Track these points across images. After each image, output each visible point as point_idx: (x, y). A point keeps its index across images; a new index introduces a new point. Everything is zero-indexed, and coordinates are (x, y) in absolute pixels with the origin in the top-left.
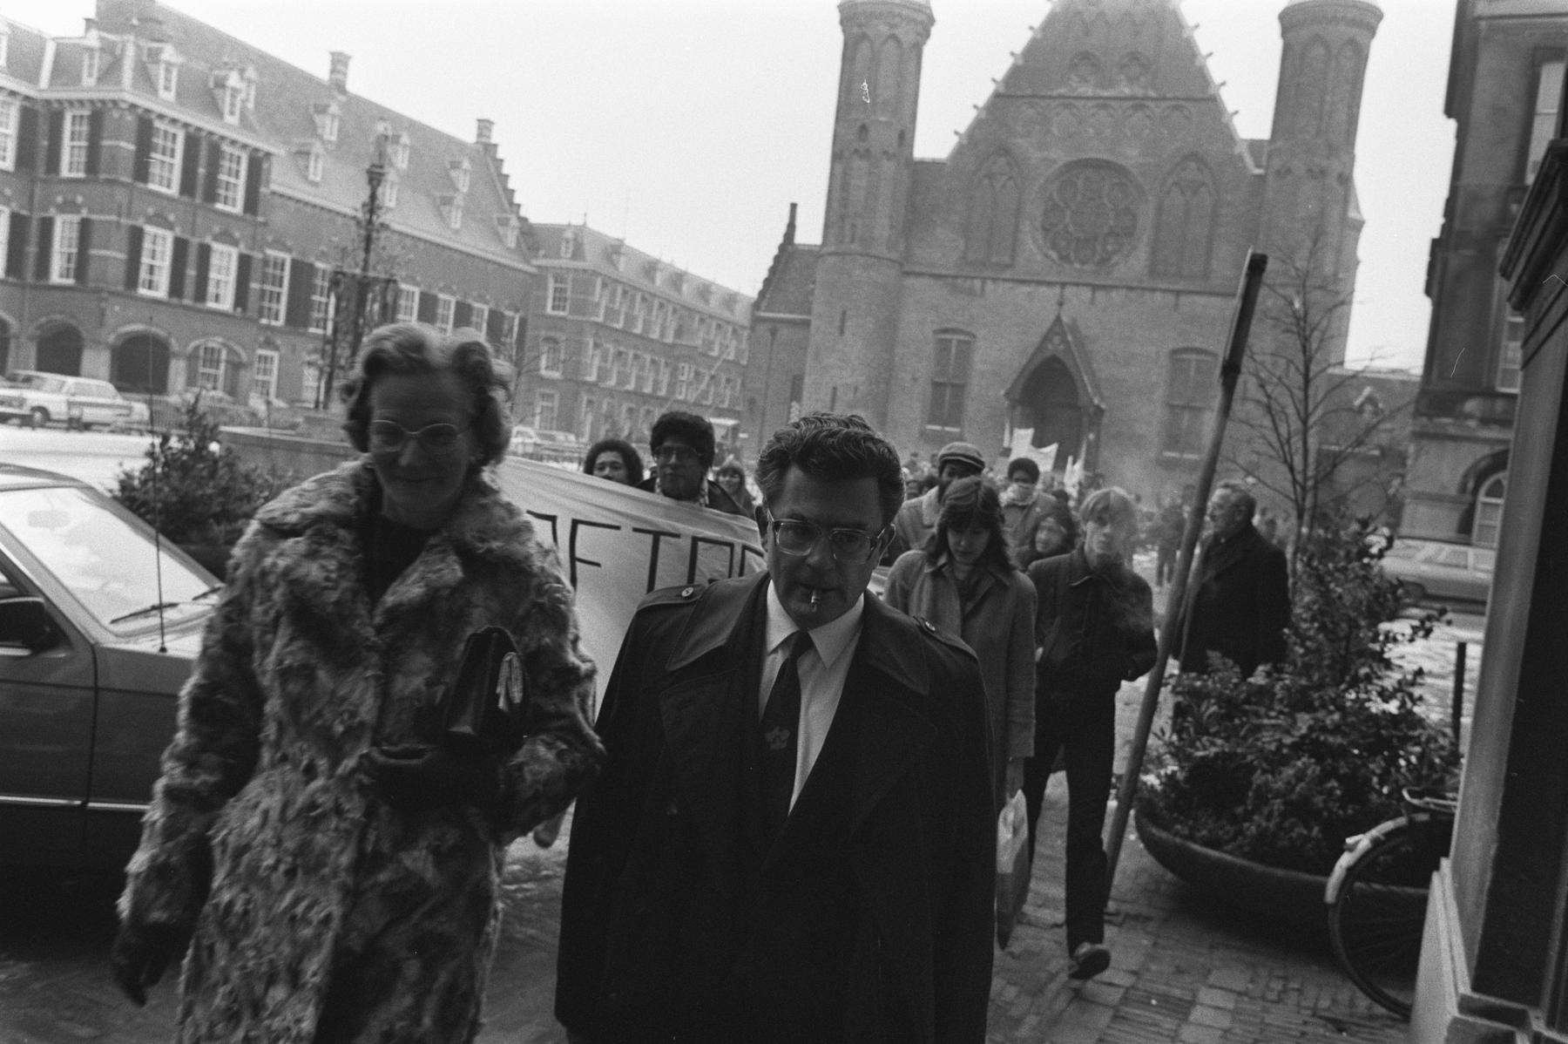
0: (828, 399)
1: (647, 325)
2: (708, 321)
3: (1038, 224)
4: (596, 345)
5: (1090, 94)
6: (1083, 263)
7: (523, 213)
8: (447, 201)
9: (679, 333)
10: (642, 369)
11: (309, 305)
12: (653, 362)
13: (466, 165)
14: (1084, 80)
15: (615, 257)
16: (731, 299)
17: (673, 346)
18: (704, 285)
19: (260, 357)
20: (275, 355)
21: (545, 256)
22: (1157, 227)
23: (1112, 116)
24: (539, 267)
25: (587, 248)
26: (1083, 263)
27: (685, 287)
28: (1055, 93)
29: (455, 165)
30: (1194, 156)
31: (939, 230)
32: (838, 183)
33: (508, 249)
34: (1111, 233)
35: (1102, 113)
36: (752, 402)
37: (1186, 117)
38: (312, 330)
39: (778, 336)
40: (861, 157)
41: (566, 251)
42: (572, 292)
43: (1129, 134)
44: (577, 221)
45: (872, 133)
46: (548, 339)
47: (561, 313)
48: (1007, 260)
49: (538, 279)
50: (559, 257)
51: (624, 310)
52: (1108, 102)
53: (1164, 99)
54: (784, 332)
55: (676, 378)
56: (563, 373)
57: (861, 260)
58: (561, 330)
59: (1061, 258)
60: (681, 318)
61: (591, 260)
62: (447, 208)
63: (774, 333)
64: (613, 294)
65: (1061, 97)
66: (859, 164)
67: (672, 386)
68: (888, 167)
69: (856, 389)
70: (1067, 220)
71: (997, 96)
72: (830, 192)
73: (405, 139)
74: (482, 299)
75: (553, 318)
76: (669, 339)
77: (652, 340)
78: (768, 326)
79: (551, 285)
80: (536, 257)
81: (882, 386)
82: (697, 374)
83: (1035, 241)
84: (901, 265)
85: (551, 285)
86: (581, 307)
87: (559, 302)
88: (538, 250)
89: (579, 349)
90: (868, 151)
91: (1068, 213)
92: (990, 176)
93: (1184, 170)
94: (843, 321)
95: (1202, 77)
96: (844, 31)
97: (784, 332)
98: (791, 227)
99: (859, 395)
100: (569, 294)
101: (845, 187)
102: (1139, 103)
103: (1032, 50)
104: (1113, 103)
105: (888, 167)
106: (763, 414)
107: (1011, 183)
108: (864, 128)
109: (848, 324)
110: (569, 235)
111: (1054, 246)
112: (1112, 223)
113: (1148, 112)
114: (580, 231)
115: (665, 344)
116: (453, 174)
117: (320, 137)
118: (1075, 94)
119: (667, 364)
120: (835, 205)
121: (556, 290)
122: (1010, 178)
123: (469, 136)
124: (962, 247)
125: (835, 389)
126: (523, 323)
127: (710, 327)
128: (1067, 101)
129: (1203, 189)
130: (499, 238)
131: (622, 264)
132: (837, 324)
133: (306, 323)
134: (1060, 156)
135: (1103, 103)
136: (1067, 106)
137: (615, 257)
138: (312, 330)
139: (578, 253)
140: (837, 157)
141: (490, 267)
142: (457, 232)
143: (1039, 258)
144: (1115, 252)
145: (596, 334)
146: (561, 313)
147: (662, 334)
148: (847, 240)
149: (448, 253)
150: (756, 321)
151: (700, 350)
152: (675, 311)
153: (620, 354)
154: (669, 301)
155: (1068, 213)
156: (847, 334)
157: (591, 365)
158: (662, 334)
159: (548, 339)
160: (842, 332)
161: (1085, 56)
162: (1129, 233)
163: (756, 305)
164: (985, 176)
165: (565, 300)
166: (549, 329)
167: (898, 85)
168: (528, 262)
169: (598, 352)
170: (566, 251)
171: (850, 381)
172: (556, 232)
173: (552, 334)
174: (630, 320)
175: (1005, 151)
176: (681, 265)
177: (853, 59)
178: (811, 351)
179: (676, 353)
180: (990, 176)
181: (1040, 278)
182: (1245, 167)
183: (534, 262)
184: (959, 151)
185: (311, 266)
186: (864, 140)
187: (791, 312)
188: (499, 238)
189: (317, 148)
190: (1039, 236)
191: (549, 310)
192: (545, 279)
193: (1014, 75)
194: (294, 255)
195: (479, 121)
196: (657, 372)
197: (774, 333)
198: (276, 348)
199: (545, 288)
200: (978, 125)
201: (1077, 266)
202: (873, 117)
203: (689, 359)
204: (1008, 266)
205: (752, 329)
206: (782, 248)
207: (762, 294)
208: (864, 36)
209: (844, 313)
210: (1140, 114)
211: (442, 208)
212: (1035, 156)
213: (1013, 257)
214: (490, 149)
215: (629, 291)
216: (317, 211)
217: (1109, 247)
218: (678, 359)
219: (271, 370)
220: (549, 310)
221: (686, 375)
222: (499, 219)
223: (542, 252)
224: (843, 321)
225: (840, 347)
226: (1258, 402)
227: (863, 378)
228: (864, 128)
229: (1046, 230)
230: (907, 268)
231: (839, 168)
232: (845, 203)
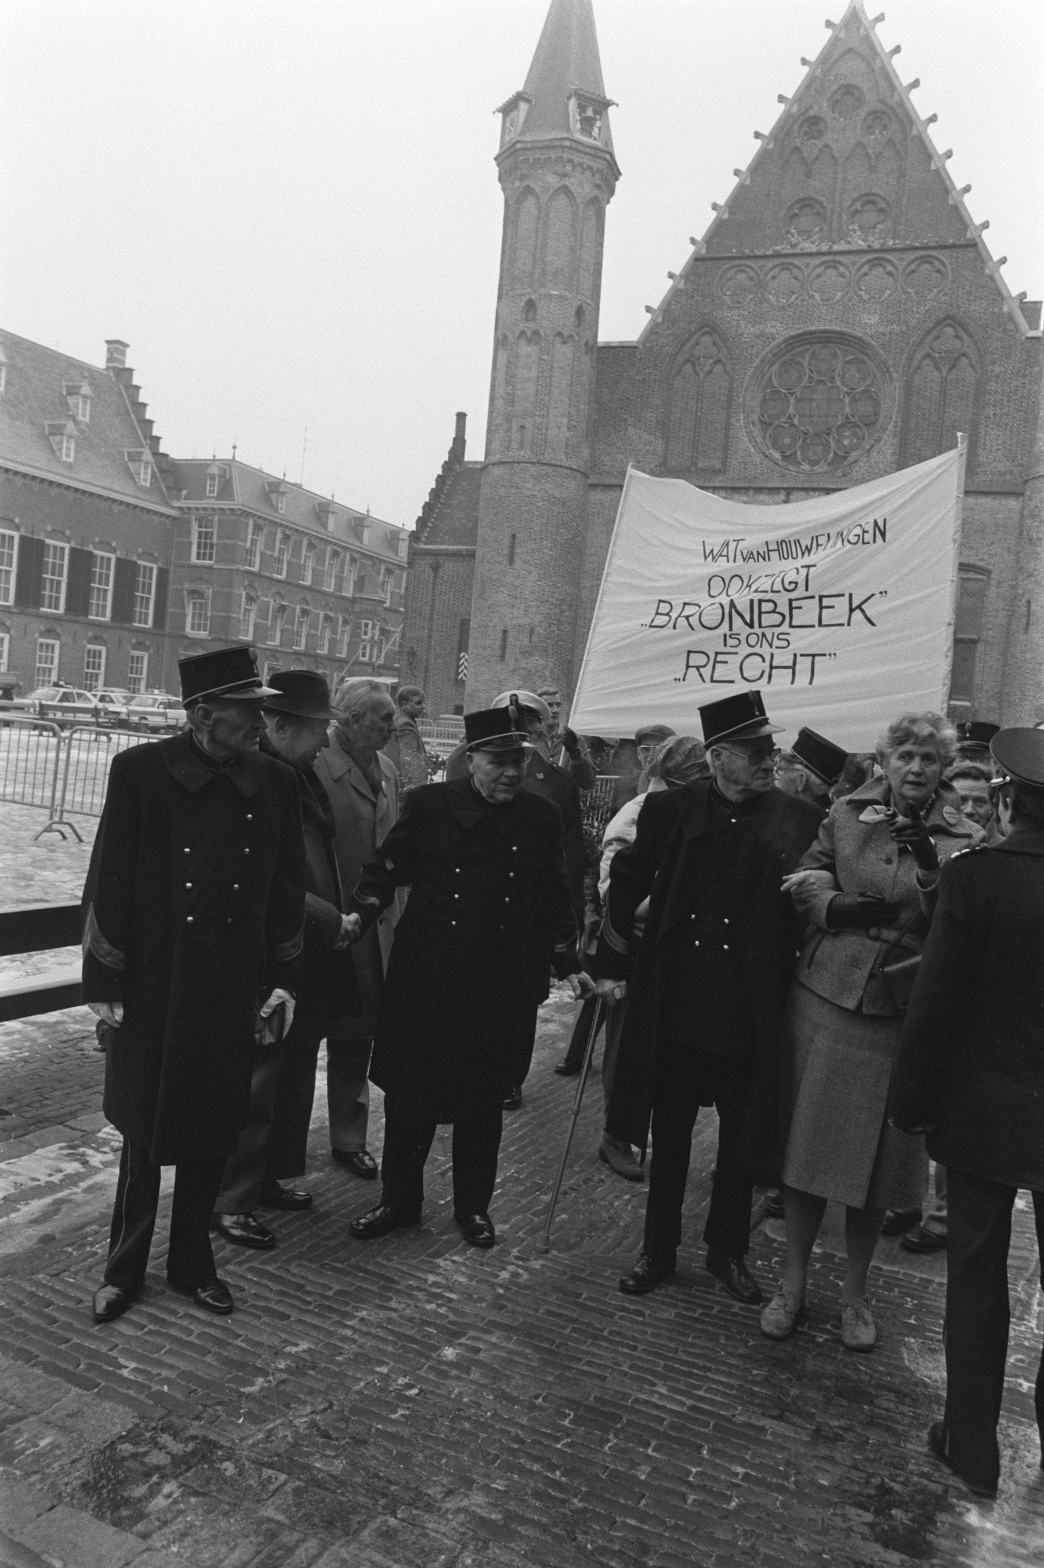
0: (498, 643)
1: (318, 576)
2: (295, 537)
3: (755, 417)
4: (251, 599)
5: (813, 248)
6: (812, 464)
7: (163, 449)
8: (57, 430)
9: (360, 585)
10: (314, 626)
11: (40, 583)
12: (327, 618)
13: (86, 390)
14: (806, 234)
15: (273, 497)
16: (392, 536)
17: (354, 600)
18: (320, 505)
19: (41, 645)
20: (57, 644)
21: (186, 498)
22: (906, 412)
23: (842, 276)
24: (181, 509)
25: (236, 485)
26: (812, 464)
27: (366, 534)
28: (770, 252)
29: (73, 391)
30: (950, 320)
31: (632, 432)
32: (501, 378)
33: (141, 488)
34: (848, 423)
35: (831, 273)
36: (412, 653)
37: (938, 271)
38: (44, 610)
39: (441, 572)
40: (529, 341)
41: (212, 489)
42: (219, 537)
43: (865, 297)
44: (225, 454)
45: (541, 311)
46: (193, 593)
47: (207, 562)
48: (718, 465)
49: (179, 524)
50: (205, 497)
51: (286, 557)
52: (838, 258)
53: (907, 249)
54: (449, 567)
55: (358, 636)
56: (210, 633)
57: (533, 469)
58: (209, 582)
59: (784, 457)
60: (363, 567)
61: (242, 497)
62: (58, 438)
63: (436, 568)
64: (272, 536)
65: (777, 255)
66: (527, 350)
67: (353, 646)
68: (564, 353)
69: (532, 631)
70: (791, 410)
71: (697, 259)
72: (493, 387)
73: (86, 390)
74: (105, 545)
75: (196, 567)
76: (349, 593)
77: (325, 594)
78: (431, 560)
79: (195, 529)
80: (179, 499)
81: (566, 628)
82: (383, 631)
83: (752, 438)
84: (586, 476)
85: (195, 529)
86: (229, 554)
87: (206, 547)
88: (180, 490)
89: (227, 602)
90: (536, 333)
91: (792, 400)
92: (692, 361)
93: (938, 337)
94: (512, 547)
95: (958, 216)
96: (504, 190)
97: (449, 567)
98: (459, 442)
99: (535, 638)
100: (215, 540)
101: (510, 380)
102: (877, 257)
103: (739, 199)
104: (844, 259)
105: (564, 353)
106: (427, 669)
107: (719, 368)
108: (531, 305)
109: (518, 550)
110: (214, 470)
111: (775, 445)
112: (847, 410)
113: (890, 268)
114: (230, 464)
115: (344, 598)
116: (71, 400)
117: (75, 420)
118: (797, 251)
119: (345, 622)
120: (499, 403)
121: (200, 534)
122: (719, 361)
123: (98, 359)
124: (660, 449)
125: (505, 632)
126: (163, 574)
127: (343, 562)
128: (785, 260)
129: (964, 360)
130: (131, 477)
131: (283, 506)
132: (506, 551)
133: (38, 602)
134: (780, 330)
135: (831, 259)
136: (785, 267)
137: (273, 497)
138: (44, 610)
139: (226, 489)
140: (500, 343)
141: (116, 508)
142: (70, 466)
143: (758, 459)
144: (853, 447)
145: (251, 585)
146: (207, 562)
147: (339, 587)
148: (514, 445)
149: (54, 491)
150: (414, 554)
151: (387, 605)
152: (353, 560)
153: (283, 608)
154: (346, 549)
155: (792, 400)
156: (518, 562)
157: (322, 637)
158: (339, 587)
159: (193, 593)
160: (511, 561)
161: (806, 203)
162: (870, 423)
163: (414, 536)
164: (687, 361)
165: (212, 545)
166: (194, 580)
167: (572, 249)
168: (167, 504)
169: (254, 607)
170: (212, 489)
171: (522, 621)
172: (199, 467)
173: (196, 587)
174: (296, 569)
175: (709, 327)
176: (274, 469)
177: (515, 223)
178: (477, 586)
179: (358, 608)
180: (692, 361)
181: (760, 484)
182: (1017, 328)
183: (176, 504)
184: (652, 332)
185: (42, 543)
186: (534, 320)
187: (458, 544)
188: (131, 477)
189: (70, 428)
190: (757, 432)
191: (194, 560)
192: (188, 522)
193: (718, 231)
194: (160, 564)
195: (108, 342)
196: (334, 631)
197: (436, 568)
198: (58, 637)
199: (189, 533)
200: (674, 297)
201: (806, 467)
202: (542, 291)
203: (373, 615)
204: (717, 472)
205: (411, 564)
206: (447, 466)
207: (421, 522)
208: (529, 190)
209: (514, 536)
210: (878, 271)
211: (51, 438)
212: (749, 330)
213: (725, 461)
214: (124, 374)
215: (291, 534)
216: (45, 485)
217: (846, 442)
218: (359, 615)
219: (99, 664)
220: (194, 560)
221: (372, 632)
222: (129, 454)
223: (184, 492)
224: (512, 547)
225: (509, 579)
226: (919, 266)
227: (539, 618)
228: (531, 305)
229: (765, 425)
230: (592, 480)
231: (503, 356)
232: (511, 400)
